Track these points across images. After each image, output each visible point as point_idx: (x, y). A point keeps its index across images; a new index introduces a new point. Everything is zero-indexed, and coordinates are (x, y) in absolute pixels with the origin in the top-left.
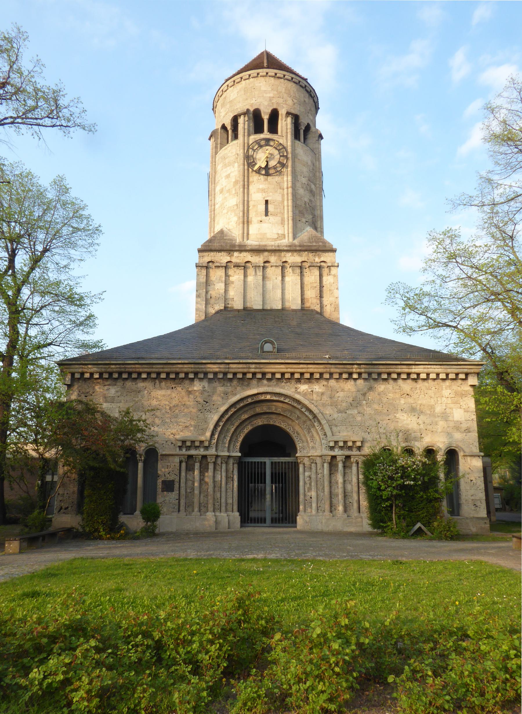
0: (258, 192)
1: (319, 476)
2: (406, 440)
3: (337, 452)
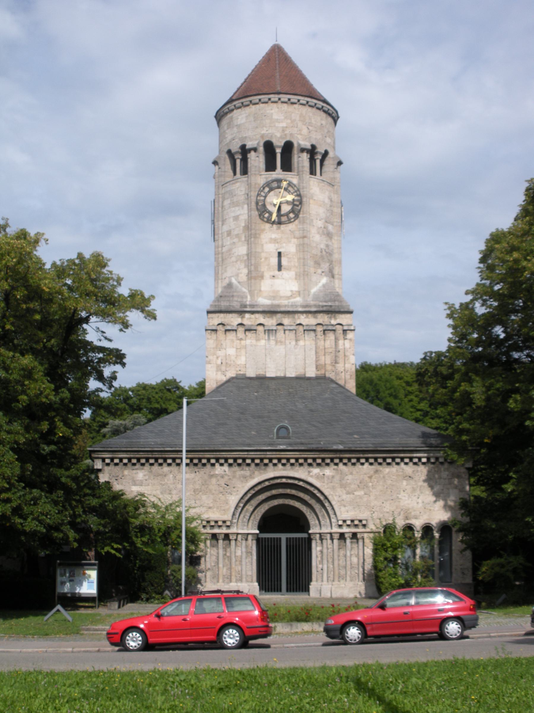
0: (270, 242)
1: (329, 550)
2: (407, 518)
3: (345, 530)
